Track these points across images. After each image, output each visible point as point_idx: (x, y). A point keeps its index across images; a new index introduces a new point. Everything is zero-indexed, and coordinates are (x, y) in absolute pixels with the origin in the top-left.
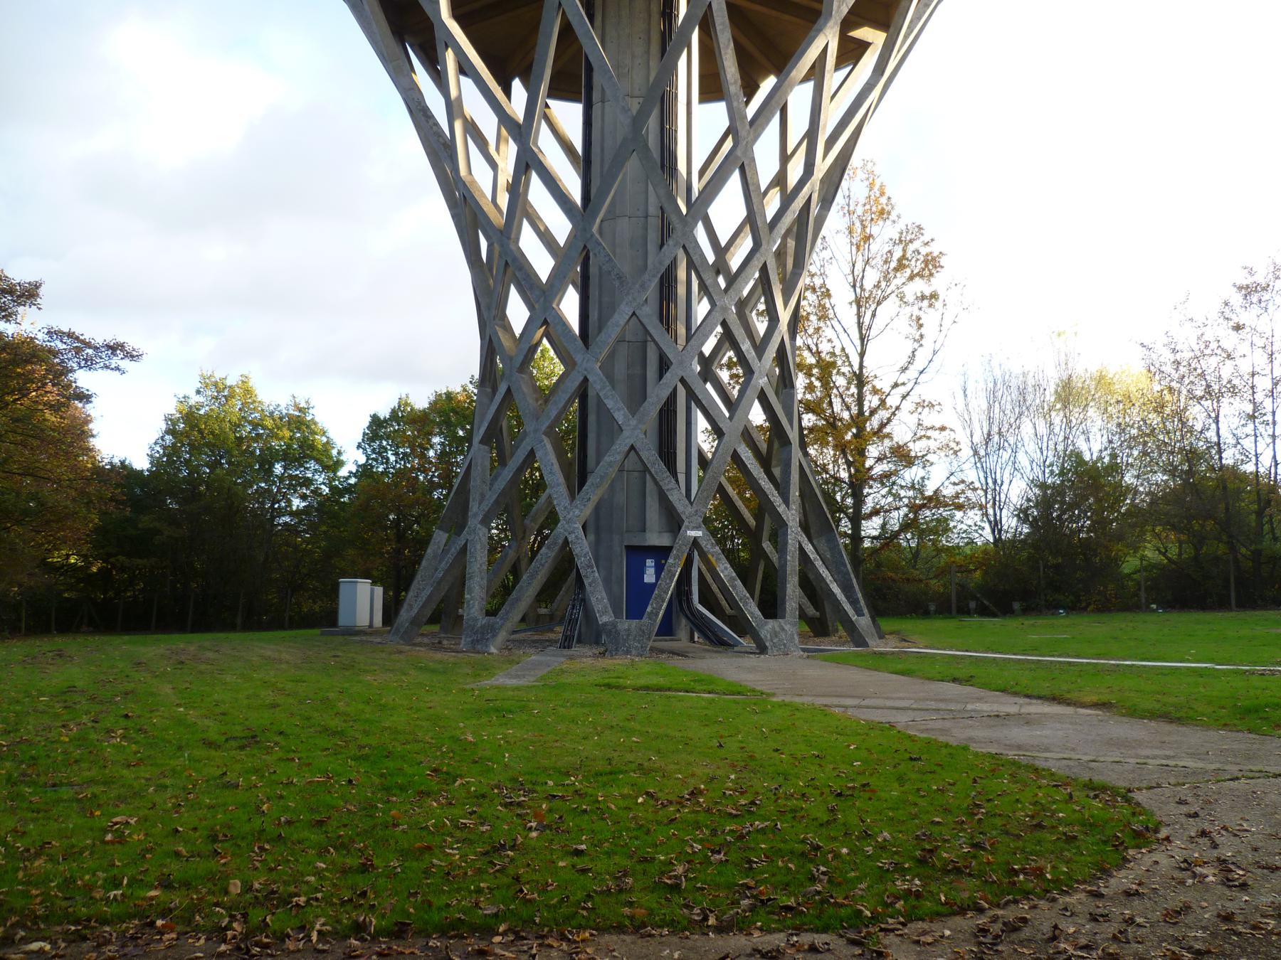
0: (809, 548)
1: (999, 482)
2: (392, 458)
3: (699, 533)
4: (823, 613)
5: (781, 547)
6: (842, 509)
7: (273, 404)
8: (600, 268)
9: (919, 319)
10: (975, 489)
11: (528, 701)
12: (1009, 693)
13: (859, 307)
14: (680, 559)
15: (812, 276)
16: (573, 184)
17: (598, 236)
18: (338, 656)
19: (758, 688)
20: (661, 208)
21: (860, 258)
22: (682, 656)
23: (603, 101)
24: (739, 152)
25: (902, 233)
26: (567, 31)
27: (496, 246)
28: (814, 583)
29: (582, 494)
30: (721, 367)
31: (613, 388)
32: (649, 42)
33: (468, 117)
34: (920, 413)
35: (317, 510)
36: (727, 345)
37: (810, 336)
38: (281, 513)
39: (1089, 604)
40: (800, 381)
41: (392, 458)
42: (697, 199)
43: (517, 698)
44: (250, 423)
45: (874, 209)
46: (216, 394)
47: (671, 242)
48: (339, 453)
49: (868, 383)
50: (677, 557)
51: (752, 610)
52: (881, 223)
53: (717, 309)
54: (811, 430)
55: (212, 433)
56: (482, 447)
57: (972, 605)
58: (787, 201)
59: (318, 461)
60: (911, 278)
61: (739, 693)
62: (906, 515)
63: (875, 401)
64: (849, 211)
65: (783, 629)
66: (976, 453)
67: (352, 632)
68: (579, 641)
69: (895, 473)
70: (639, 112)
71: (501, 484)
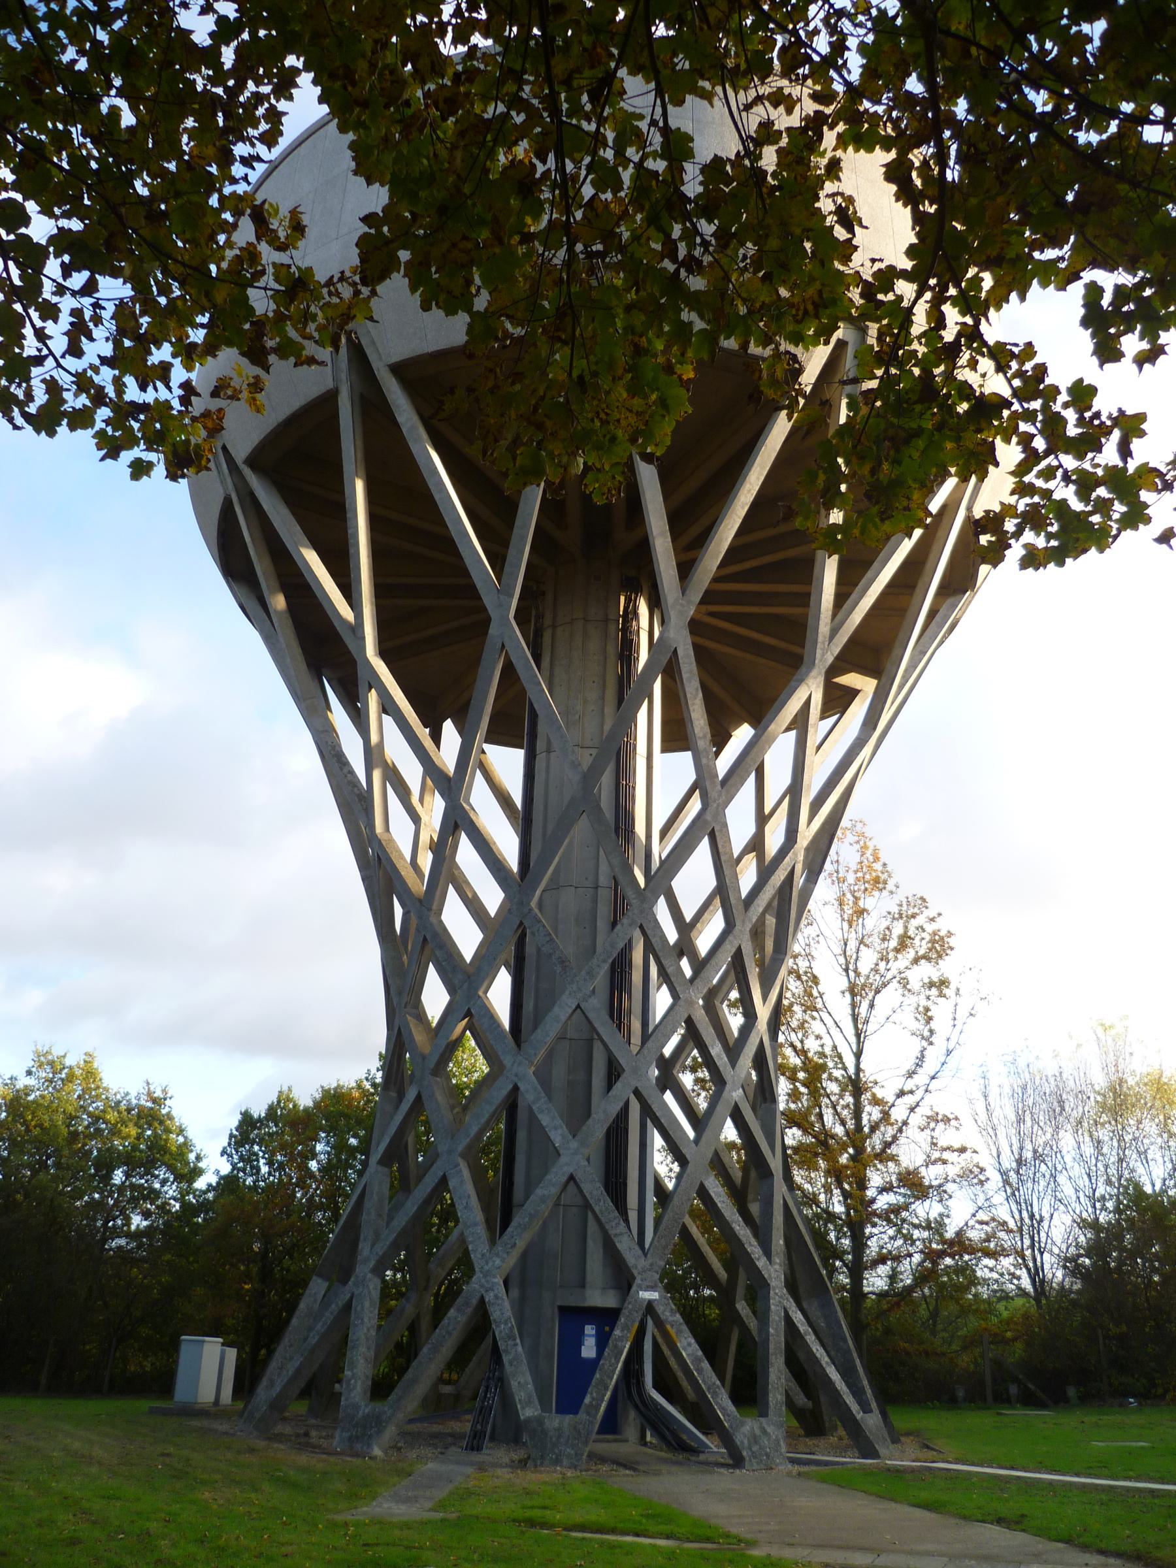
0: (798, 1317)
1: (1037, 1217)
2: (264, 1169)
3: (654, 1295)
4: (816, 1402)
5: (762, 1316)
6: (838, 1254)
7: (122, 1091)
8: (539, 950)
9: (927, 1010)
10: (1009, 1231)
11: (421, 1548)
12: (1076, 1546)
13: (853, 994)
14: (629, 1330)
15: (795, 957)
16: (508, 844)
17: (537, 911)
18: (168, 1455)
19: (734, 1530)
20: (614, 878)
21: (853, 935)
22: (630, 1468)
23: (549, 751)
24: (708, 817)
25: (901, 905)
26: (509, 670)
27: (413, 916)
28: (806, 1366)
29: (505, 1237)
30: (684, 1069)
31: (550, 1099)
32: (604, 687)
33: (389, 762)
34: (933, 1130)
35: (162, 1232)
36: (691, 1044)
37: (793, 1030)
38: (116, 1233)
39: (1166, 1391)
40: (783, 1086)
41: (264, 1169)
42: (659, 869)
43: (406, 1543)
44: (90, 1115)
45: (868, 877)
46: (51, 1075)
47: (625, 921)
48: (199, 1158)
49: (866, 1090)
50: (626, 1327)
51: (723, 1403)
52: (876, 893)
53: (681, 1003)
54: (796, 1150)
55: (41, 1126)
56: (380, 1168)
57: (1013, 1390)
58: (765, 873)
59: (171, 1168)
60: (916, 961)
61: (708, 1540)
62: (920, 1264)
63: (876, 1114)
64: (838, 879)
65: (765, 1432)
66: (1006, 1182)
67: (191, 1411)
68: (493, 1438)
69: (906, 1207)
70: (592, 767)
71: (402, 1219)
